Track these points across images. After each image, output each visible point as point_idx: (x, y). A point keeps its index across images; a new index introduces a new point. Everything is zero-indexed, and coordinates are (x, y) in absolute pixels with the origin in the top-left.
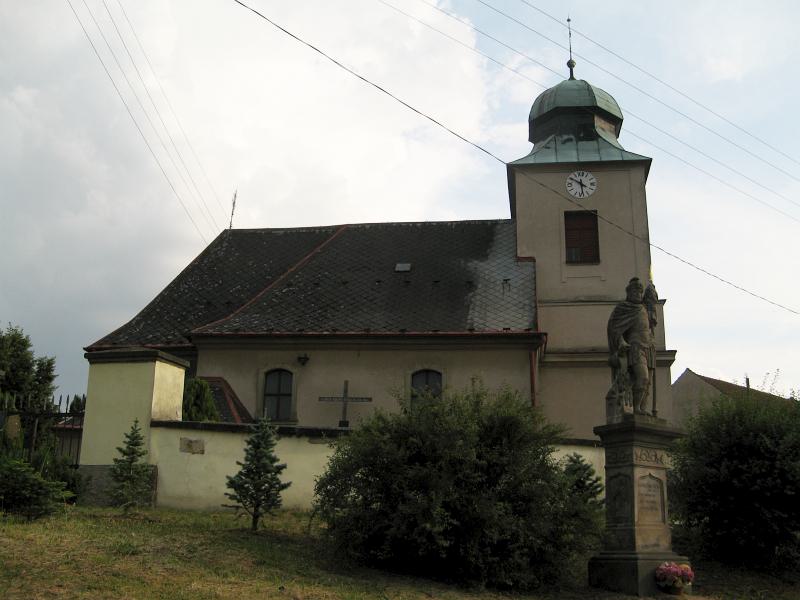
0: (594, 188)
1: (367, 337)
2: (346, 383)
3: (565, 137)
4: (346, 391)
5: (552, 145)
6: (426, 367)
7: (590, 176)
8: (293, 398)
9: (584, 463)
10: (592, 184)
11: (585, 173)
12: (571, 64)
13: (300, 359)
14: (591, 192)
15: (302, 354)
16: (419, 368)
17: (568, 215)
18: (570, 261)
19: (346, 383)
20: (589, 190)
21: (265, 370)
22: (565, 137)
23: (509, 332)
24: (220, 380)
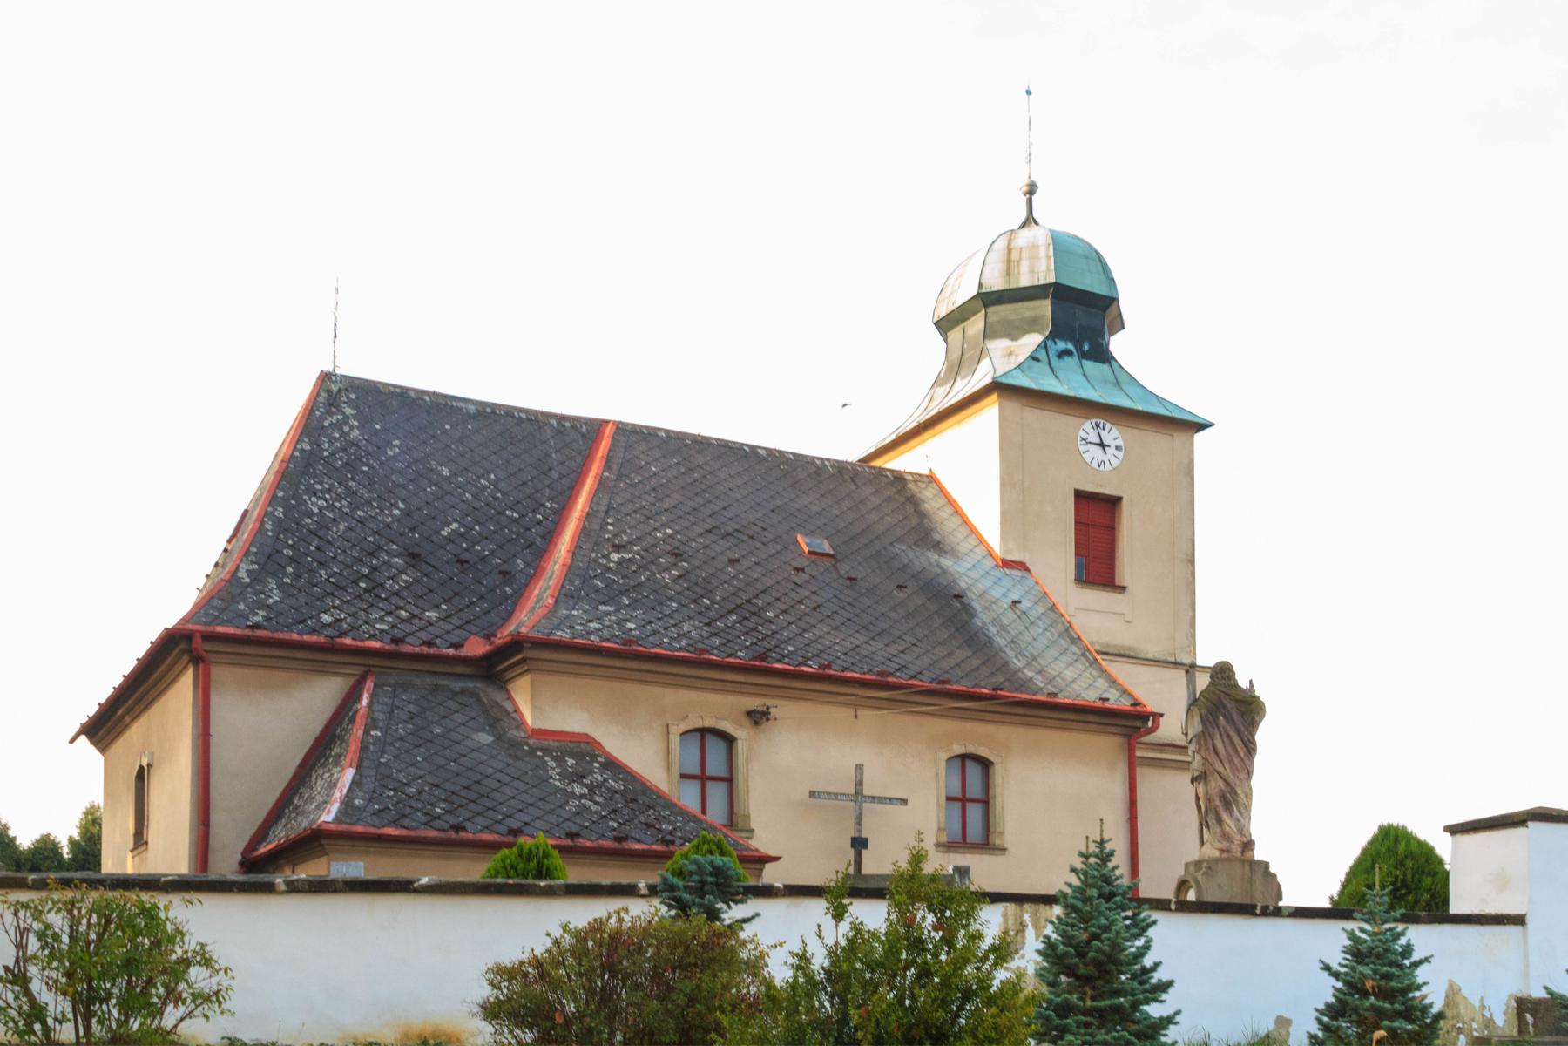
0: (1120, 454)
2: (859, 768)
4: (859, 783)
7: (1115, 432)
9: (819, 961)
10: (1117, 448)
11: (1108, 426)
12: (1031, 190)
13: (750, 714)
14: (1115, 463)
15: (756, 703)
17: (1081, 497)
18: (1079, 580)
19: (859, 768)
20: (1112, 458)
21: (683, 727)
23: (1107, 705)
24: (588, 740)
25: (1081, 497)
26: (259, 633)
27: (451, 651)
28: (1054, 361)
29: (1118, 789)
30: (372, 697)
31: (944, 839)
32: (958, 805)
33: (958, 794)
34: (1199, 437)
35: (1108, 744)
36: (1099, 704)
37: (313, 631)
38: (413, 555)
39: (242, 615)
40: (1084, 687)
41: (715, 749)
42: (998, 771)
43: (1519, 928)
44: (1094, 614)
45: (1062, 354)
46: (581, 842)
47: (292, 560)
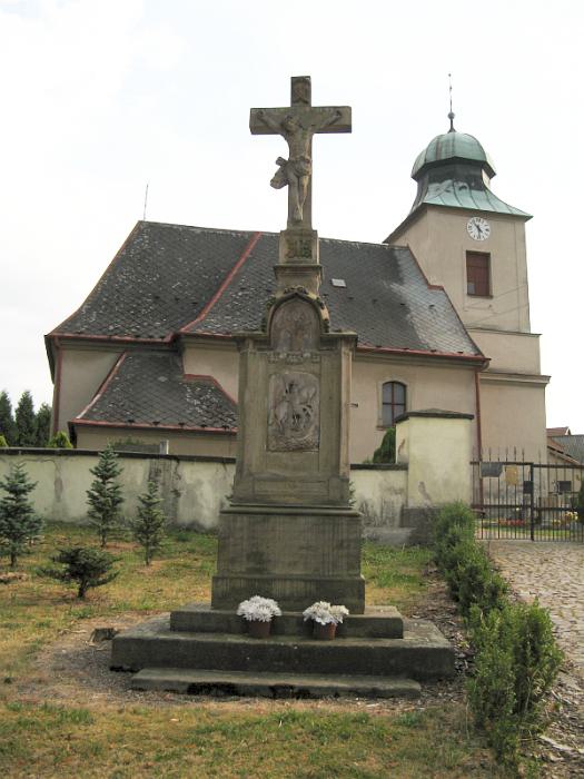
1: (110, 341)
3: (461, 184)
5: (451, 189)
6: (396, 379)
7: (485, 223)
8: (381, 402)
12: (451, 116)
16: (388, 379)
17: (469, 254)
22: (461, 184)
24: (209, 378)
25: (469, 254)
26: (82, 336)
27: (160, 340)
28: (457, 193)
29: (472, 397)
30: (122, 364)
31: (381, 424)
32: (389, 407)
33: (390, 401)
34: (527, 224)
35: (465, 374)
36: (458, 355)
37: (104, 334)
38: (157, 298)
39: (78, 328)
40: (451, 345)
41: (398, 390)
42: (409, 389)
43: (402, 473)
44: (474, 311)
45: (461, 189)
46: (185, 427)
47: (106, 303)
